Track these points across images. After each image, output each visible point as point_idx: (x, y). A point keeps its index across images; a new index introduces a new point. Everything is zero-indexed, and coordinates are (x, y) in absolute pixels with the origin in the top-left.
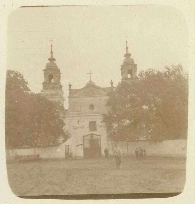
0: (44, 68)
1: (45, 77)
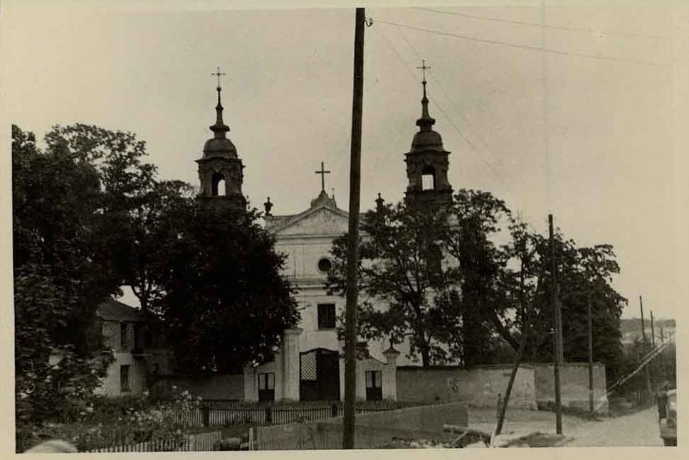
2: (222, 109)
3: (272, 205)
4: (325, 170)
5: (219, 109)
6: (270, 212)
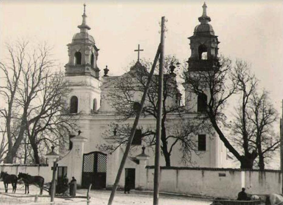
0: (192, 34)
1: (192, 48)
2: (203, 7)
3: (108, 70)
4: (140, 49)
5: (84, 16)
6: (107, 75)
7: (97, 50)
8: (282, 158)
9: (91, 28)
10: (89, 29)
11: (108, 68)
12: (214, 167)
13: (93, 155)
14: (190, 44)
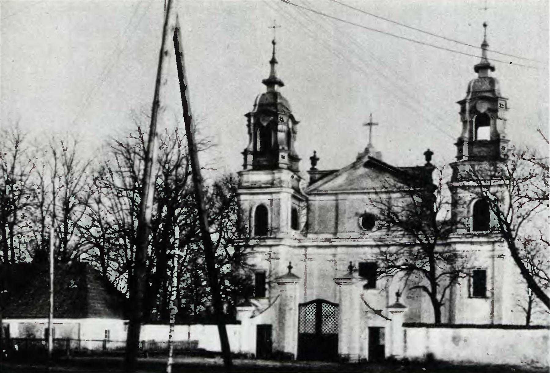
0: (250, 109)
3: (318, 159)
7: (295, 123)
8: (117, 316)
9: (285, 84)
10: (281, 84)
11: (318, 155)
12: (418, 321)
13: (314, 305)
14: (460, 113)
